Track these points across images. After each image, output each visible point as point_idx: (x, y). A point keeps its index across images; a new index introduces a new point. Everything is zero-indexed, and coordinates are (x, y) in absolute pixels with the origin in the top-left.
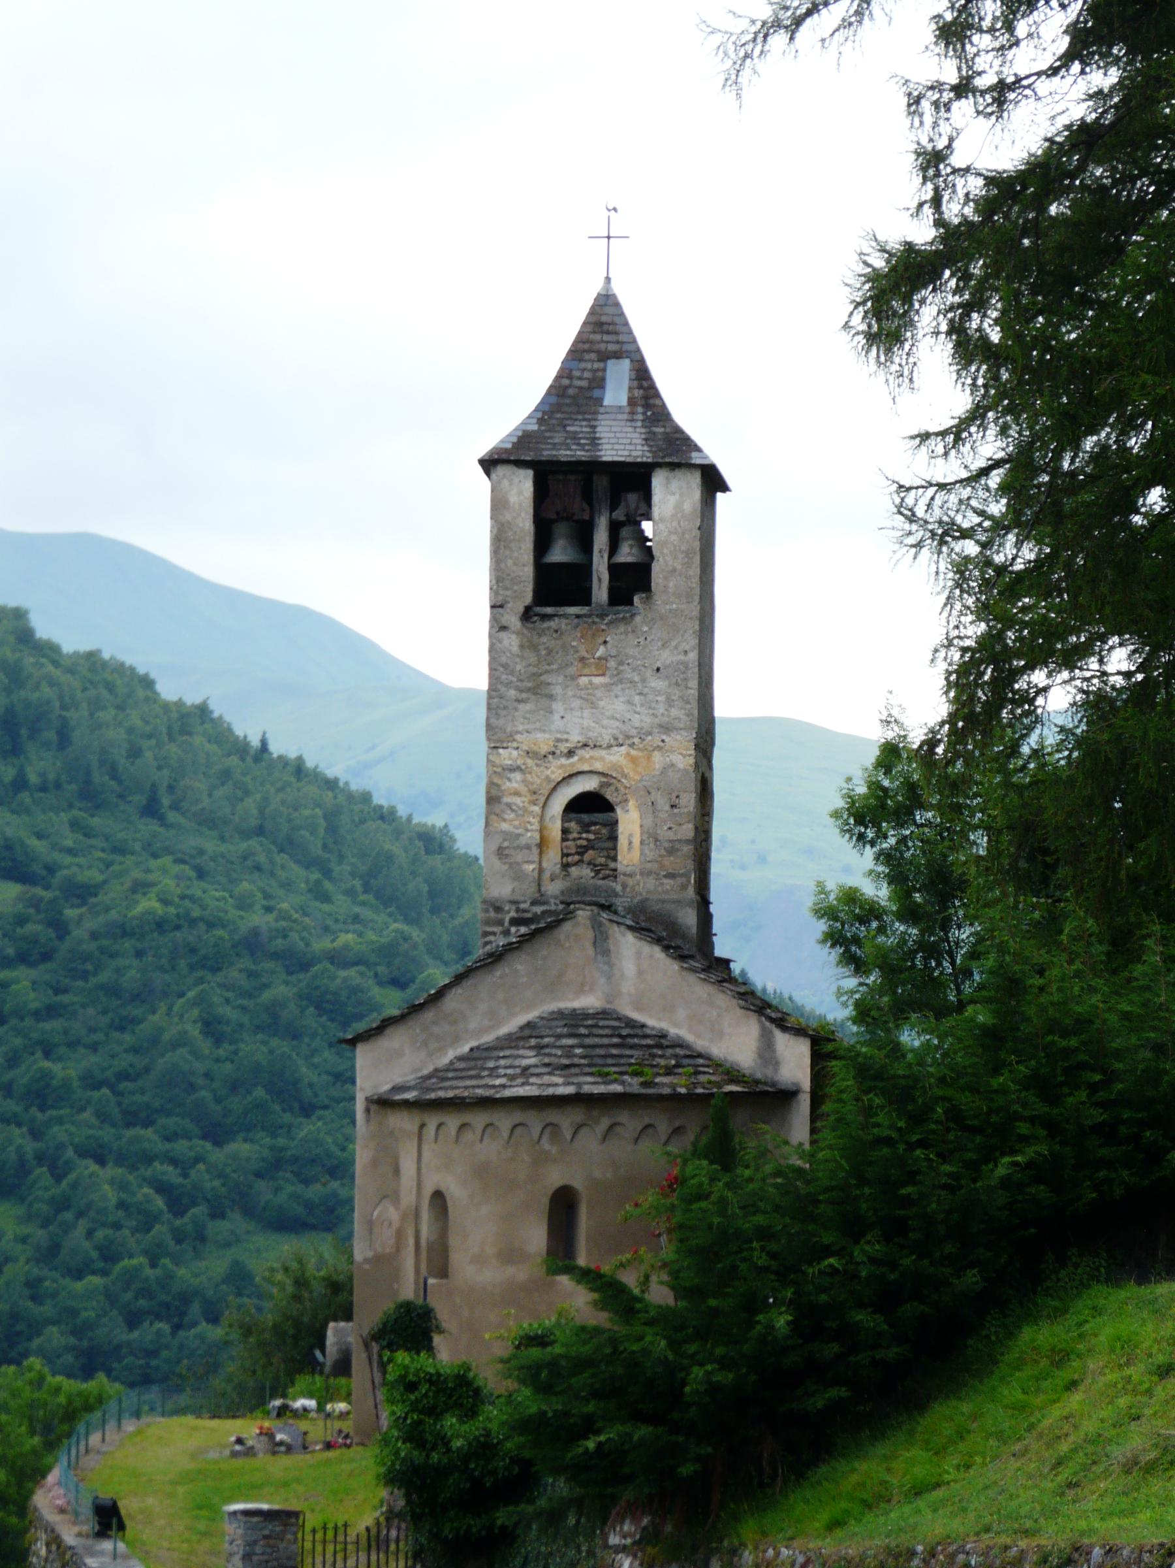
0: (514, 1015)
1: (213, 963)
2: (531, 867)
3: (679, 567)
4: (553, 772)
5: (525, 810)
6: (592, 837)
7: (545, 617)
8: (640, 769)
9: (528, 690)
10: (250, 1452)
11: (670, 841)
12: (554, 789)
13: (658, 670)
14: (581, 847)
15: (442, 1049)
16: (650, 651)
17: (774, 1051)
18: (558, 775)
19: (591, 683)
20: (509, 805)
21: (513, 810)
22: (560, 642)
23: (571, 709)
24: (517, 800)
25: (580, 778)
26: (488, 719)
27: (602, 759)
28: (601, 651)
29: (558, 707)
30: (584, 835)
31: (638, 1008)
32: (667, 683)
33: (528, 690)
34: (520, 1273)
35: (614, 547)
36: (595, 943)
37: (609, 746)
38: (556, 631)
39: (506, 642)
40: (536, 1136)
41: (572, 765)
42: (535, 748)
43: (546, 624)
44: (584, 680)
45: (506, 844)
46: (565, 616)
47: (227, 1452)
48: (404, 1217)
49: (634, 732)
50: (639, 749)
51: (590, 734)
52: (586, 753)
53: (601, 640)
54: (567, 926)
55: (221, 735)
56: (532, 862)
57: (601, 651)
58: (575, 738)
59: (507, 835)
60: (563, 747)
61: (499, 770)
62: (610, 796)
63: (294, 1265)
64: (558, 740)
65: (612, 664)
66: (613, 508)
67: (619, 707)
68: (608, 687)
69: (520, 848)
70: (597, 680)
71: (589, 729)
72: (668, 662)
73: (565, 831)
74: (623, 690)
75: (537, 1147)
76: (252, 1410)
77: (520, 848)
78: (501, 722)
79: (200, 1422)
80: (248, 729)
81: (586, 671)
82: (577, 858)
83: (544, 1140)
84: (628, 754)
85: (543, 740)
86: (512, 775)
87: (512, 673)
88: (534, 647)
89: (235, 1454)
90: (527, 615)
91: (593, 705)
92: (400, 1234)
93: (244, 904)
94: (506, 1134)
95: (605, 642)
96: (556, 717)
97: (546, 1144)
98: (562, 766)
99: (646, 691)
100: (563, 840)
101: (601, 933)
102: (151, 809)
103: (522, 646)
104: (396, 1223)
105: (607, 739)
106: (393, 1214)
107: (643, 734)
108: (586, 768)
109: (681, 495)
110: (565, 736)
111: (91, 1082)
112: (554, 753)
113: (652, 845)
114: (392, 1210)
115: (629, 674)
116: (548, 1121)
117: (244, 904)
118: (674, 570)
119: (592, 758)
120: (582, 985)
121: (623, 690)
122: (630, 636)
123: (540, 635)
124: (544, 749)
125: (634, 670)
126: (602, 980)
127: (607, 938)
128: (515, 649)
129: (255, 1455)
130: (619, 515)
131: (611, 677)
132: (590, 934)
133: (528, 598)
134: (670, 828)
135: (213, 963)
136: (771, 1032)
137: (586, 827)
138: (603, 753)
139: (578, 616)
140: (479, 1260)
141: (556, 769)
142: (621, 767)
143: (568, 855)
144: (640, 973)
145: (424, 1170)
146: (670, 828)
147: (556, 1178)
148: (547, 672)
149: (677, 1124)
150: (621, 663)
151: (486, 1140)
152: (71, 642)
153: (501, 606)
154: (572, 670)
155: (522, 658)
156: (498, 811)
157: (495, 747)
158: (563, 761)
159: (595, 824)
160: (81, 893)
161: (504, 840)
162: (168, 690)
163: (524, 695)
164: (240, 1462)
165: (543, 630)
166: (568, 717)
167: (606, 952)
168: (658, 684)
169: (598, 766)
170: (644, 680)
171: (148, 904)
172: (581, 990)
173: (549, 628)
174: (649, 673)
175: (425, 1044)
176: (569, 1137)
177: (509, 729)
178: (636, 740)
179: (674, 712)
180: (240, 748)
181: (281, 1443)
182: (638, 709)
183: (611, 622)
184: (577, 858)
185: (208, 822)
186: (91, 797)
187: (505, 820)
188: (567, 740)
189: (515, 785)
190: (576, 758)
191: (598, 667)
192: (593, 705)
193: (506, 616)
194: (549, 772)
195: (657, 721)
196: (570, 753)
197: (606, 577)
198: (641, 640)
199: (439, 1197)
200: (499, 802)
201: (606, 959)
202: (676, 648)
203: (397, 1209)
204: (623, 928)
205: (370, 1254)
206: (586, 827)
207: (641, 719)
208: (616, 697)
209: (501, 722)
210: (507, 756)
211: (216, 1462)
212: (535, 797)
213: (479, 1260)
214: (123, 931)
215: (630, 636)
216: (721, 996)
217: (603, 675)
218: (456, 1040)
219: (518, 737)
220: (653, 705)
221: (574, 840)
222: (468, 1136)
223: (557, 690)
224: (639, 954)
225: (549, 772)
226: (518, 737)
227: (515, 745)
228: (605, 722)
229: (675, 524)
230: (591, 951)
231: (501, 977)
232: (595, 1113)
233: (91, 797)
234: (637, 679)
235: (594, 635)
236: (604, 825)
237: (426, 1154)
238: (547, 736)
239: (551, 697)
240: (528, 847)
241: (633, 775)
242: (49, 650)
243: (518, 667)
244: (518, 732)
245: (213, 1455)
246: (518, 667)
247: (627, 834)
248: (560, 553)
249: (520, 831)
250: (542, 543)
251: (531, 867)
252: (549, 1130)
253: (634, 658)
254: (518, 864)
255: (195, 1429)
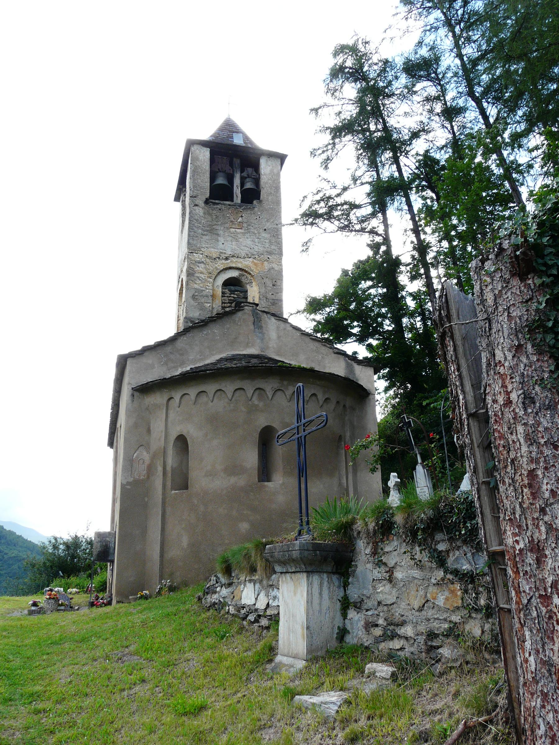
0: (213, 355)
1: (20, 561)
2: (209, 305)
3: (273, 192)
4: (219, 266)
5: (206, 280)
6: (236, 296)
7: (215, 204)
8: (258, 268)
9: (207, 231)
10: (41, 611)
11: (273, 299)
12: (219, 273)
13: (265, 230)
14: (231, 300)
15: (176, 368)
16: (262, 222)
17: (354, 374)
18: (221, 267)
19: (236, 231)
20: (198, 277)
21: (200, 280)
22: (222, 214)
23: (227, 241)
24: (202, 276)
25: (230, 271)
26: (188, 240)
27: (241, 262)
28: (240, 220)
29: (221, 240)
30: (232, 295)
31: (278, 355)
32: (269, 235)
33: (207, 231)
34: (241, 481)
35: (242, 184)
36: (254, 323)
37: (244, 258)
38: (220, 210)
39: (197, 211)
40: (249, 395)
41: (228, 263)
42: (211, 255)
43: (215, 206)
44: (232, 230)
45: (196, 294)
46: (224, 204)
47: (26, 612)
48: (154, 457)
49: (255, 253)
50: (258, 260)
51: (236, 252)
52: (234, 260)
53: (240, 215)
54: (240, 314)
55: (23, 538)
56: (209, 303)
57: (240, 220)
58: (229, 252)
59: (197, 290)
60: (223, 256)
61: (194, 262)
62: (243, 279)
63: (53, 541)
64: (221, 253)
65: (245, 225)
66: (242, 172)
67: (249, 242)
68: (244, 234)
69: (203, 296)
70: (238, 231)
71: (235, 249)
72: (270, 227)
73: (223, 293)
74: (250, 236)
75: (250, 403)
76: (36, 593)
77: (203, 296)
78: (195, 242)
79: (11, 598)
80: (25, 538)
81: (233, 226)
82: (229, 305)
83: (254, 398)
84: (253, 262)
85: (214, 253)
86: (200, 265)
87: (200, 223)
88: (210, 215)
89: (31, 613)
90: (207, 202)
91: (237, 240)
92: (150, 469)
93: (24, 555)
94: (230, 395)
95: (242, 216)
96: (220, 243)
97: (255, 401)
98: (223, 264)
99: (260, 237)
100: (222, 296)
101: (257, 318)
102: (15, 545)
103: (204, 213)
104: (147, 462)
105: (243, 254)
106: (146, 456)
107: (260, 254)
108: (234, 265)
109: (273, 167)
110: (224, 251)
111: (5, 574)
112: (219, 258)
113: (265, 301)
114: (145, 453)
115: (252, 230)
116: (258, 386)
117: (24, 555)
118: (271, 193)
119: (236, 261)
120: (248, 344)
121: (250, 236)
122: (253, 215)
123: (213, 210)
124: (215, 256)
125: (255, 229)
126: (258, 341)
127: (261, 320)
128: (202, 214)
129: (45, 613)
130: (245, 174)
131: (245, 230)
132: (252, 319)
133: (208, 195)
134: (272, 294)
135: (20, 561)
136: (352, 365)
137: (232, 292)
138: (242, 260)
139: (229, 205)
140: (211, 474)
141: (221, 265)
142: (250, 266)
143: (225, 303)
144: (279, 337)
145: (170, 424)
146: (272, 294)
147: (262, 421)
148: (216, 225)
149: (327, 397)
150: (249, 225)
151: (215, 400)
152: (8, 529)
153: (195, 197)
154: (227, 225)
155: (205, 218)
156: (193, 279)
157: (191, 253)
158: (223, 261)
159: (237, 291)
160: (6, 554)
161: (196, 292)
162: (17, 534)
163: (205, 233)
164: (35, 618)
165: (214, 208)
166: (225, 244)
167: (261, 327)
168: (264, 235)
169: (240, 266)
170: (259, 233)
171: (13, 555)
172: (247, 346)
173: (217, 208)
174: (261, 231)
175: (166, 363)
176: (270, 397)
177: (198, 246)
178: (256, 256)
179: (273, 247)
180: (24, 539)
181: (62, 605)
182: (257, 244)
183: (244, 209)
184: (229, 305)
185: (21, 547)
186: (9, 545)
187: (196, 284)
188: (225, 253)
189: (201, 269)
190: (229, 261)
191: (238, 225)
192: (237, 240)
193: (197, 201)
194: (217, 266)
195: (265, 249)
196: (227, 259)
197: (240, 196)
198: (258, 217)
199: (182, 441)
200: (194, 276)
201: (260, 331)
202: (273, 222)
203: (148, 452)
204: (269, 315)
205: (131, 480)
206: (232, 292)
207: (258, 248)
208: (247, 238)
209: (195, 242)
210: (197, 257)
211: (19, 619)
212: (211, 275)
213: (211, 474)
214: (10, 558)
215: (253, 215)
216: (324, 348)
217: (241, 229)
218: (183, 364)
219: (202, 249)
220: (264, 243)
221: (227, 297)
222: (204, 398)
223: (221, 232)
224: (278, 328)
225: (217, 266)
226: (202, 249)
227: (201, 252)
228: (242, 248)
229: (270, 176)
230: (252, 327)
231: (206, 335)
232: (285, 383)
233: (9, 545)
234: (256, 232)
235: (237, 213)
236: (241, 292)
237: (172, 415)
238: (216, 250)
239: (218, 235)
240: (207, 296)
241: (255, 271)
242: (5, 530)
243: (203, 221)
244: (202, 247)
245: (17, 614)
246: (203, 221)
247: (252, 296)
248: (221, 180)
249: (203, 289)
250: (213, 178)
251: (209, 305)
252: (257, 392)
253: (255, 224)
254: (202, 303)
255: (8, 601)
